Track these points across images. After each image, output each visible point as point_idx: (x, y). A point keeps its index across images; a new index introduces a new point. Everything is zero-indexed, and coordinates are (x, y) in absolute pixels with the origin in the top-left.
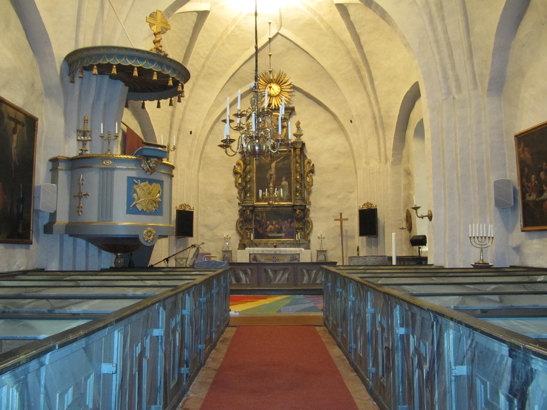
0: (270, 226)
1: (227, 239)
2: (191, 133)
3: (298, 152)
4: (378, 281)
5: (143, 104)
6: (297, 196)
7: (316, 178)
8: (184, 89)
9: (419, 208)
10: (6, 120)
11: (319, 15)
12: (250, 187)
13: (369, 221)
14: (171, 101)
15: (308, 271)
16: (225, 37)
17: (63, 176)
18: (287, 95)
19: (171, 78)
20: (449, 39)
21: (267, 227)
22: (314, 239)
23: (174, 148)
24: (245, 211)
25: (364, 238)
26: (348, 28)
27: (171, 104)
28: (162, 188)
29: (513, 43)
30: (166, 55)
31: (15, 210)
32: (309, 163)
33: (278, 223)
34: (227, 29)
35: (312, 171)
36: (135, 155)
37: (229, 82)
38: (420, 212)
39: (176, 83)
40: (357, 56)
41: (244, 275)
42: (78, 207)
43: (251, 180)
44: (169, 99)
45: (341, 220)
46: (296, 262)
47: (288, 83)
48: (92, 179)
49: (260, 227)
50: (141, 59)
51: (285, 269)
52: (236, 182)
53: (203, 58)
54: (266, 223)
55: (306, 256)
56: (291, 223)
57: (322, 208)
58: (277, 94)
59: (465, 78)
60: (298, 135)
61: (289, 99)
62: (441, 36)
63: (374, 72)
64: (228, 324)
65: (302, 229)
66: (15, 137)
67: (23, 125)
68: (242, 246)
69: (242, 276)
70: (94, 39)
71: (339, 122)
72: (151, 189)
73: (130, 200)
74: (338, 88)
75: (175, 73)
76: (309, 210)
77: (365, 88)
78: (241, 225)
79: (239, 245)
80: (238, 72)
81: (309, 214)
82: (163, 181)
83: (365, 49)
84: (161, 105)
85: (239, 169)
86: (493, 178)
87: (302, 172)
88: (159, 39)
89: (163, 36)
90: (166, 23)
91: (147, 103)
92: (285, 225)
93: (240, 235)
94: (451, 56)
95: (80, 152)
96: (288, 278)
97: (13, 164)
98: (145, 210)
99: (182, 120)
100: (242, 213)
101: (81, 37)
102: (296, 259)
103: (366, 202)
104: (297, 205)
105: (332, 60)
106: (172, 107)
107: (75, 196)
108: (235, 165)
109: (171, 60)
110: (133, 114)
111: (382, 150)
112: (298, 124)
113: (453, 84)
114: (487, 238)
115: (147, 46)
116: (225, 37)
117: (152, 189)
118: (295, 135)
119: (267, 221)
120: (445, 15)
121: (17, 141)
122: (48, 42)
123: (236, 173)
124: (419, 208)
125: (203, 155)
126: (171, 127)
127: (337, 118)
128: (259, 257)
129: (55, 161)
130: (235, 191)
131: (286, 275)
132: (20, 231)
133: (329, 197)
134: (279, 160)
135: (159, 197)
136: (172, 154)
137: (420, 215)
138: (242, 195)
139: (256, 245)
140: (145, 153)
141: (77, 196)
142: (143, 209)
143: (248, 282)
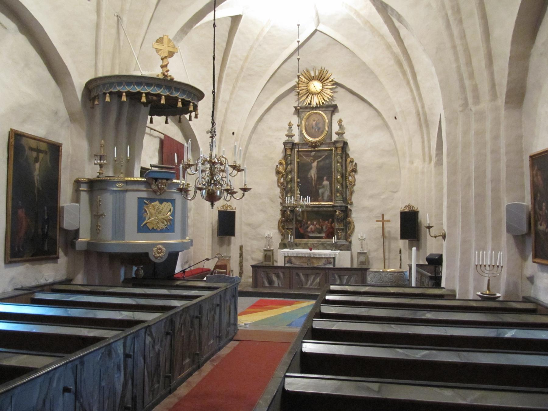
0: (311, 226)
1: (269, 238)
2: (233, 133)
3: (339, 151)
4: (334, 325)
6: (337, 196)
7: (358, 177)
9: (432, 227)
10: (27, 152)
11: (355, 10)
12: (291, 188)
13: (410, 225)
16: (261, 38)
17: (84, 197)
18: (329, 92)
20: (467, 44)
21: (308, 227)
22: (355, 239)
24: (285, 211)
26: (386, 22)
29: (533, 50)
30: (172, 80)
31: (40, 231)
32: (352, 162)
33: (319, 223)
35: (355, 171)
37: (270, 81)
38: (433, 232)
39: (186, 104)
40: (397, 50)
41: (276, 279)
43: (292, 180)
45: (383, 221)
46: (331, 266)
47: (330, 80)
48: (108, 200)
49: (301, 227)
50: (149, 85)
51: (317, 273)
52: (278, 181)
53: (240, 60)
54: (307, 223)
55: (343, 259)
56: (331, 223)
57: (364, 208)
58: (319, 91)
59: (484, 87)
61: (331, 96)
62: (458, 42)
63: (416, 68)
64: (233, 337)
65: (343, 229)
66: (37, 165)
67: (46, 153)
68: (283, 245)
69: (274, 278)
71: (383, 119)
73: (141, 218)
74: (381, 83)
76: (351, 210)
77: (408, 83)
79: (280, 244)
80: (279, 71)
83: (406, 44)
85: (281, 169)
86: (506, 201)
87: (344, 172)
88: (165, 64)
89: (170, 60)
90: (174, 47)
92: (326, 225)
93: (282, 234)
95: (98, 174)
96: (319, 282)
97: (36, 191)
99: (224, 122)
100: (283, 212)
101: (100, 65)
102: (330, 263)
103: (407, 205)
104: (337, 206)
105: (375, 54)
107: (95, 216)
112: (340, 122)
113: (470, 95)
114: (496, 267)
115: (156, 72)
117: (163, 208)
120: (463, 17)
123: (278, 172)
124: (432, 227)
125: (247, 155)
128: (293, 260)
129: (77, 183)
131: (318, 280)
133: (371, 197)
135: (170, 215)
137: (433, 235)
139: (297, 246)
141: (96, 216)
142: (153, 228)
143: (281, 286)
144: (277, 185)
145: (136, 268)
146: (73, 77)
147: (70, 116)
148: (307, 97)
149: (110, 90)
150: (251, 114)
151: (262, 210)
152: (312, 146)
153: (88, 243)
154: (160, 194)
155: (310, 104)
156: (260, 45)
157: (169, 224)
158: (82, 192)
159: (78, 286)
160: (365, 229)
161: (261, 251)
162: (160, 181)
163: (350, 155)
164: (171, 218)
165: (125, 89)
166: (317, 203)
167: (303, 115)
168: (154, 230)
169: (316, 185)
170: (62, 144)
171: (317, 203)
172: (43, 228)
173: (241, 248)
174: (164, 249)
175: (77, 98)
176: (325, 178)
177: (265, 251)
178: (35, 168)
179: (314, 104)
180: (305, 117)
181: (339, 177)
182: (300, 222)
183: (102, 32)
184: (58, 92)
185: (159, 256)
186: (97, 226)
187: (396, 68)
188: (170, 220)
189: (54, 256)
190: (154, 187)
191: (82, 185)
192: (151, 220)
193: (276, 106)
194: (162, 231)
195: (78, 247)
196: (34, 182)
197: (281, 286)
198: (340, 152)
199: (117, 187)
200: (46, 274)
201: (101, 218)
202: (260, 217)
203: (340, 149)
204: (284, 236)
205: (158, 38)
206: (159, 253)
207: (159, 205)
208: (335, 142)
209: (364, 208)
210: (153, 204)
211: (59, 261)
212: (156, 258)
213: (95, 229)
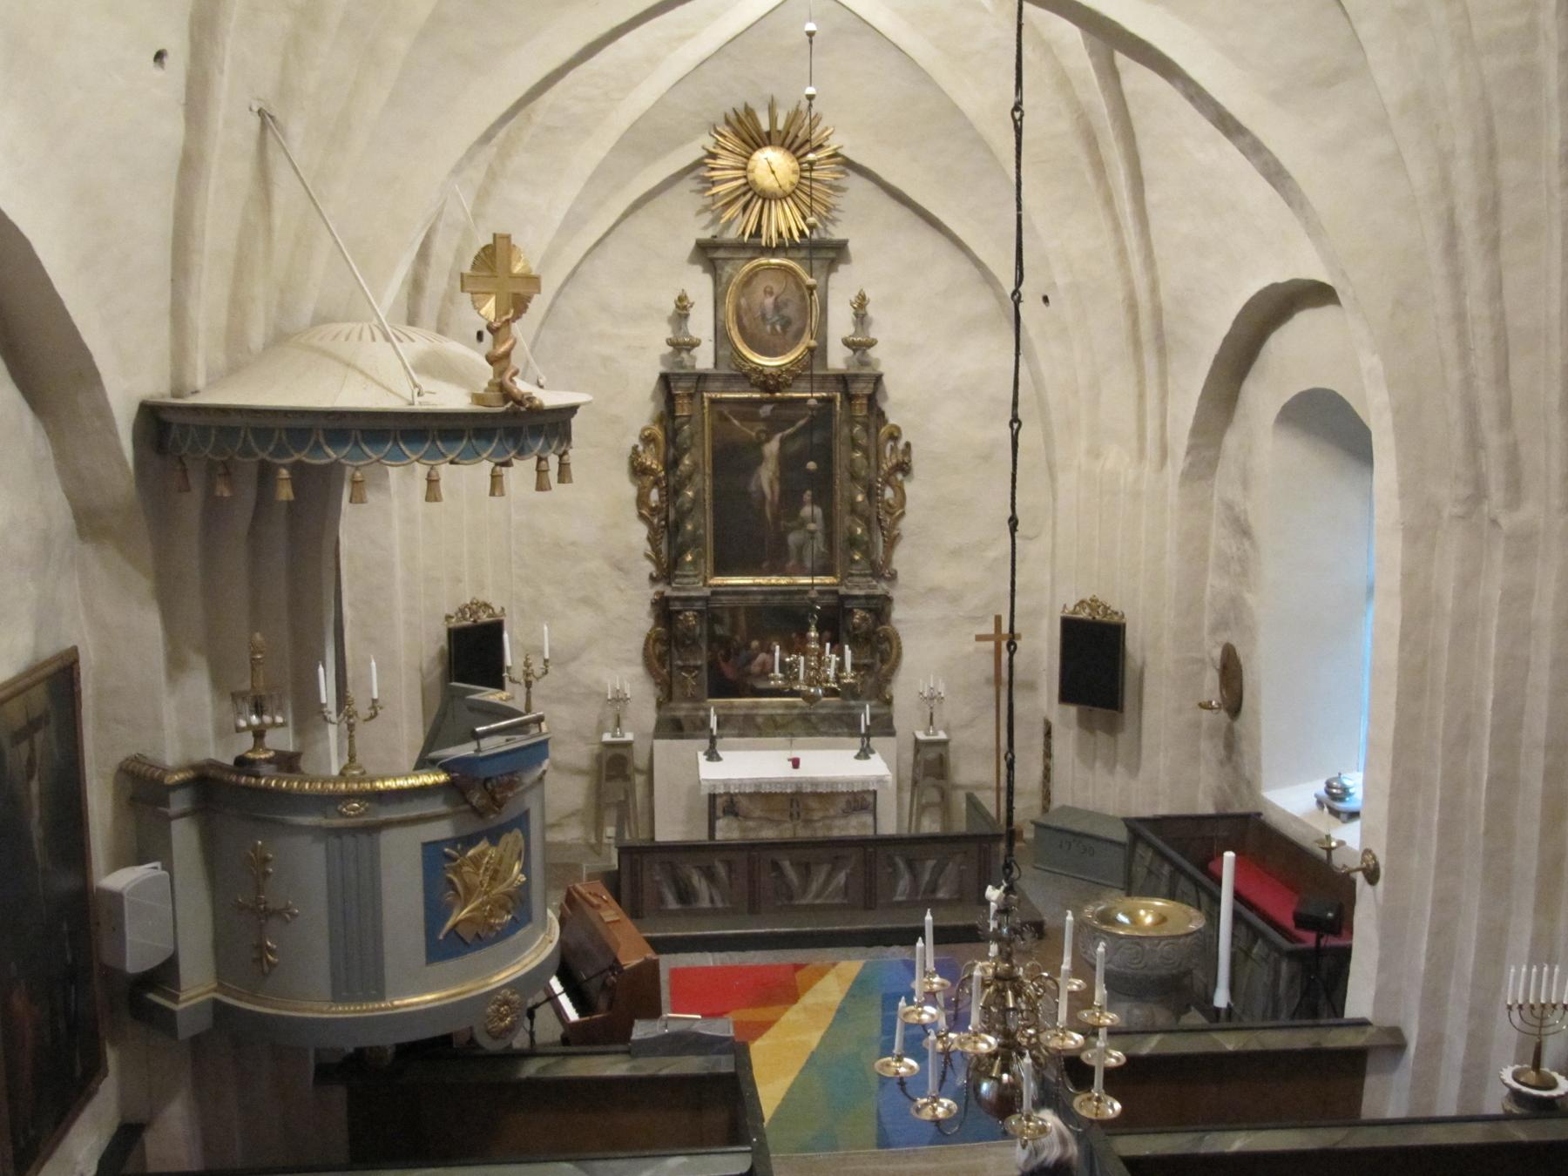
3: (860, 411)
6: (853, 561)
15: (910, 864)
17: (184, 836)
20: (1503, 315)
21: (750, 660)
25: (1072, 710)
32: (894, 436)
35: (904, 468)
49: (726, 660)
52: (642, 500)
54: (748, 646)
58: (788, 188)
60: (859, 346)
63: (1147, 164)
69: (699, 882)
70: (629, 662)
73: (435, 912)
77: (1109, 201)
78: (659, 648)
81: (889, 615)
85: (650, 461)
94: (1502, 377)
103: (1088, 598)
104: (856, 597)
111: (1152, 425)
112: (860, 305)
113: (1495, 476)
118: (847, 343)
119: (751, 638)
120: (1504, 233)
123: (638, 471)
127: (994, 277)
130: (638, 534)
131: (841, 877)
133: (956, 553)
134: (789, 431)
138: (663, 547)
142: (478, 935)
148: (745, 208)
149: (297, 457)
151: (586, 601)
152: (764, 387)
155: (757, 233)
160: (935, 657)
163: (888, 415)
166: (784, 581)
167: (728, 269)
169: (776, 518)
170: (75, 650)
171: (784, 581)
175: (123, 463)
176: (808, 495)
179: (769, 235)
180: (737, 279)
181: (860, 498)
182: (724, 642)
184: (44, 448)
187: (1077, 149)
191: (172, 796)
197: (719, 905)
198: (865, 413)
199: (342, 815)
202: (581, 622)
203: (865, 401)
204: (667, 693)
208: (843, 380)
209: (931, 590)
210: (470, 853)
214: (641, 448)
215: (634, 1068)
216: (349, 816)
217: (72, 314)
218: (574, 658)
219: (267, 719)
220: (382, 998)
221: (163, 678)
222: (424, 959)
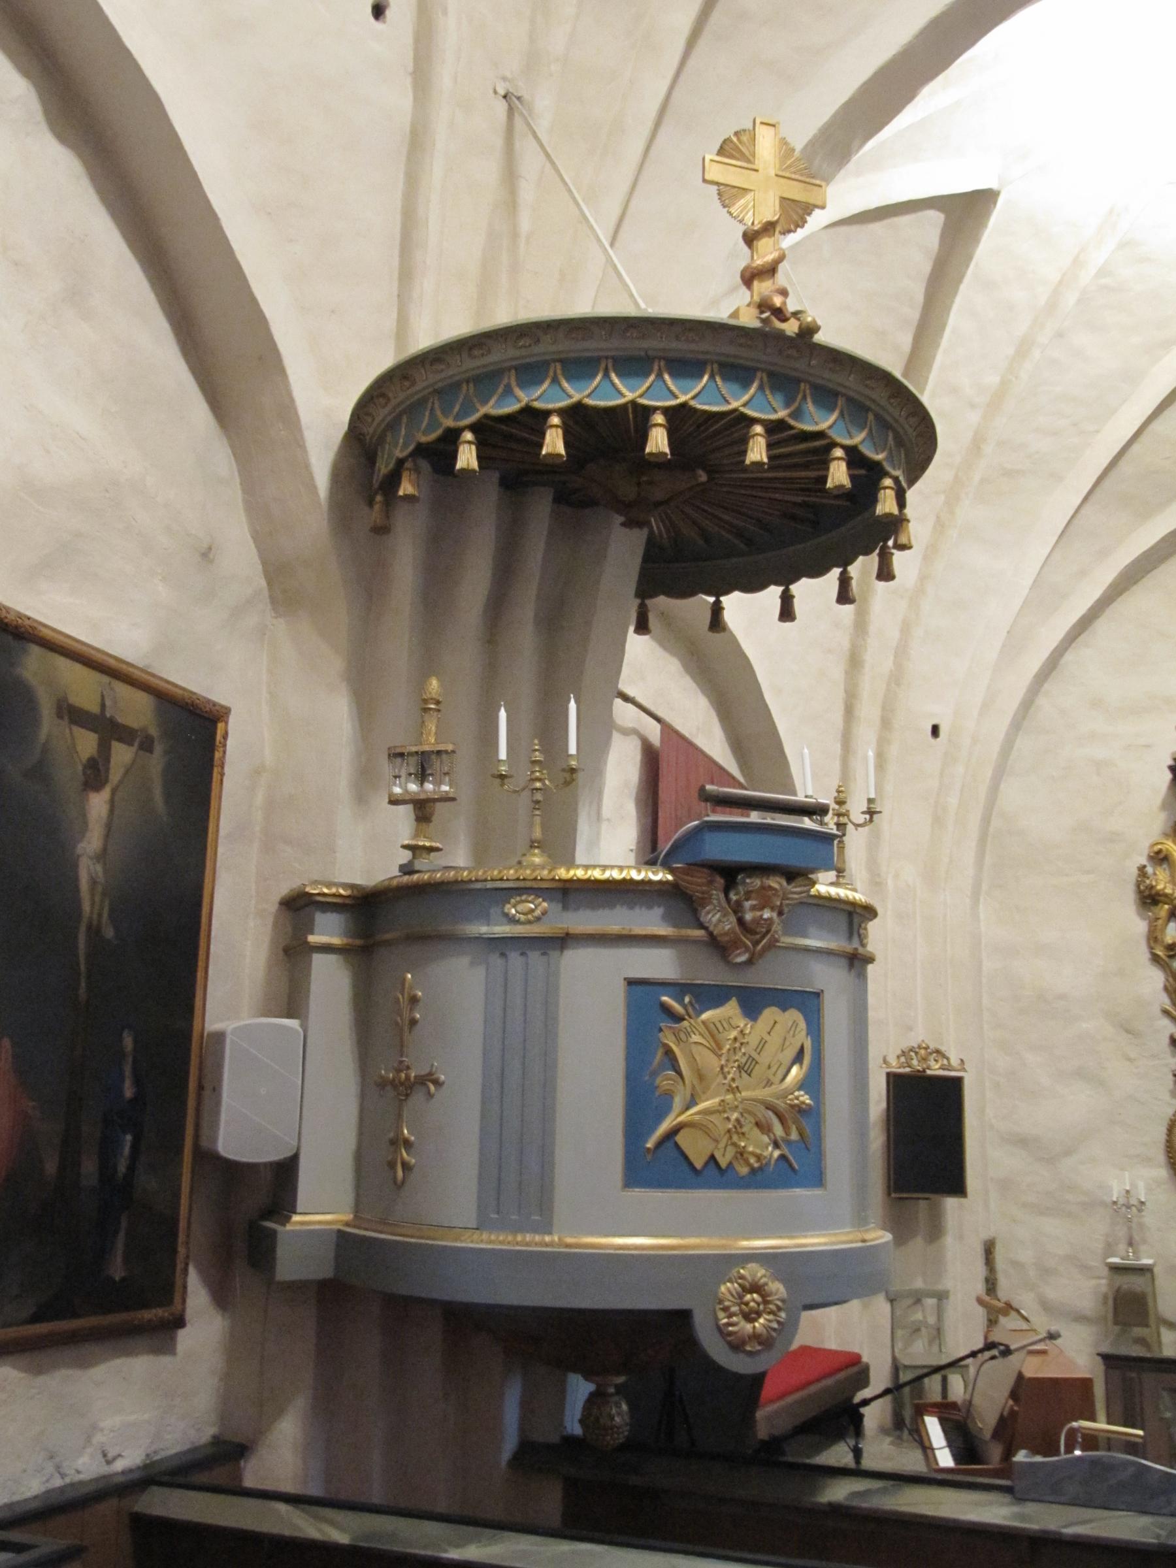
1: (1127, 1210)
2: (935, 731)
5: (717, 609)
8: (909, 511)
10: (48, 725)
14: (844, 581)
16: (1070, 299)
17: (330, 980)
19: (838, 452)
23: (871, 813)
27: (844, 596)
28: (815, 1029)
30: (808, 331)
31: (89, 1167)
34: (1077, 263)
36: (666, 865)
39: (867, 474)
42: (394, 1142)
44: (836, 572)
48: (457, 993)
52: (1153, 938)
53: (973, 406)
66: (98, 804)
67: (147, 745)
70: (1147, 1160)
72: (753, 1040)
73: (642, 1103)
75: (862, 427)
80: (1136, 448)
82: (818, 995)
84: (798, 605)
88: (770, 258)
91: (735, 605)
95: (406, 856)
98: (723, 1163)
99: (896, 678)
106: (848, 608)
107: (383, 1084)
108: (1143, 861)
109: (839, 359)
110: (688, 669)
116: (1070, 299)
117: (763, 1044)
121: (109, 826)
122: (268, 359)
125: (996, 823)
126: (849, 712)
129: (299, 906)
132: (117, 1270)
135: (802, 1085)
136: (855, 843)
140: (721, 849)
141: (392, 1086)
144: (1148, 955)
145: (591, 1387)
146: (292, 378)
147: (270, 583)
149: (484, 410)
150: (1013, 644)
153: (343, 1241)
154: (750, 962)
156: (1060, 335)
157: (794, 1136)
158: (318, 959)
159: (282, 1507)
161: (1084, 1268)
162: (756, 882)
164: (806, 1099)
165: (554, 395)
168: (715, 1174)
172: (107, 1149)
173: (989, 1250)
174: (777, 1289)
175: (312, 487)
177: (1116, 1269)
178: (84, 815)
183: (436, 172)
185: (755, 1337)
186: (399, 1142)
188: (801, 1111)
189: (159, 1313)
190: (718, 919)
192: (698, 1113)
193: (1109, 612)
194: (760, 1177)
195: (290, 1264)
196: (76, 889)
199: (512, 920)
200: (110, 1422)
201: (418, 1098)
202: (1075, 1104)
205: (729, 133)
206: (749, 1317)
207: (742, 1022)
211: (185, 1338)
212: (737, 1345)
213: (384, 1161)
214: (1149, 870)
215: (1016, 1516)
216: (518, 922)
217: (235, 246)
218: (1068, 1153)
219: (429, 786)
220: (547, 1229)
221: (343, 784)
222: (620, 1184)
